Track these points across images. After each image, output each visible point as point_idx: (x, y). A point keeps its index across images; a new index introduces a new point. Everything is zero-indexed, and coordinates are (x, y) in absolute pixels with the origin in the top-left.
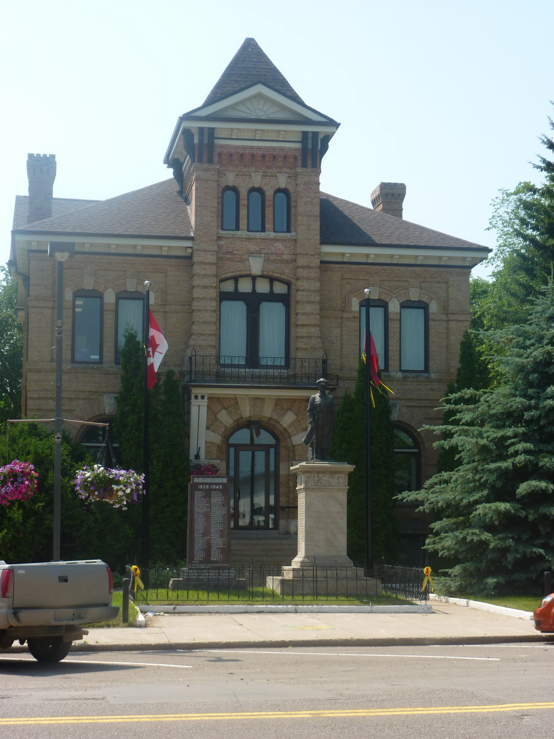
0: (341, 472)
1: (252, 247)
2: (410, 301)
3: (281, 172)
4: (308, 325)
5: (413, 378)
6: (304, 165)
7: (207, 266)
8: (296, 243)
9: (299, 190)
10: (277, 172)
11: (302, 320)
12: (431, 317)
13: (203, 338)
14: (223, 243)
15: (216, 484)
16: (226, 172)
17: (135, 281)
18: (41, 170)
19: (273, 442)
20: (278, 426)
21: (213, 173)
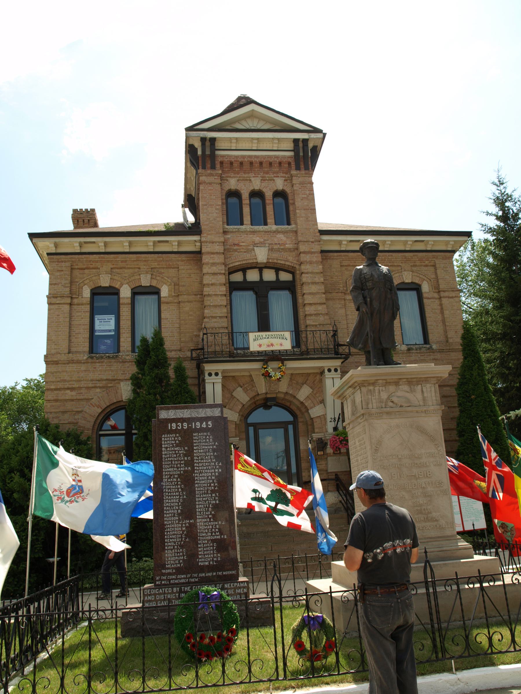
0: (426, 380)
1: (257, 239)
2: (403, 283)
3: (278, 177)
4: (315, 304)
5: (416, 350)
6: (298, 168)
7: (215, 256)
8: (296, 234)
9: (295, 188)
10: (274, 177)
11: (308, 299)
12: (425, 295)
13: (215, 320)
14: (229, 236)
15: (201, 420)
16: (228, 178)
17: (149, 276)
18: (84, 220)
19: (290, 418)
20: (295, 401)
21: (216, 177)
